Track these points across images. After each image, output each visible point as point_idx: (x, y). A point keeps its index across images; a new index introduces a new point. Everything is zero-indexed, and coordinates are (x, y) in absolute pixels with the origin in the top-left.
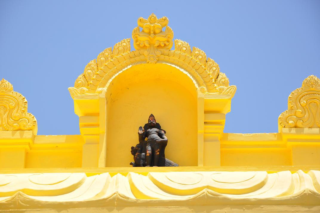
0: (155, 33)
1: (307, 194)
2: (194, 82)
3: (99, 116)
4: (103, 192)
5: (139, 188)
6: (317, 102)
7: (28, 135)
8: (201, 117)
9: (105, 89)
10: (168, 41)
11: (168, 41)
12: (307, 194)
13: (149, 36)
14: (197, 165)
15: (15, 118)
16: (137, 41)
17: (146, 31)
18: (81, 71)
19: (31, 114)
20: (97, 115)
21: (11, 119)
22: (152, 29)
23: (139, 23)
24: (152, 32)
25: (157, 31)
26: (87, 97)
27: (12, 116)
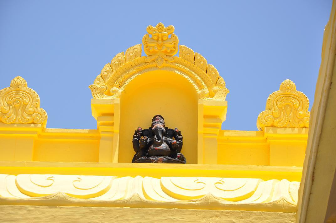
0: (163, 40)
1: (173, 144)
2: (191, 81)
3: (113, 116)
4: (8, 176)
5: (165, 186)
6: (290, 104)
7: (38, 128)
8: (201, 121)
9: (121, 90)
10: (174, 48)
11: (174, 48)
12: (173, 144)
13: (156, 42)
14: (197, 163)
15: (29, 112)
16: (147, 47)
17: (156, 38)
18: (99, 72)
19: (43, 109)
20: (112, 115)
21: (25, 112)
22: (160, 36)
23: (148, 31)
24: (160, 39)
25: (165, 38)
26: (106, 99)
27: (26, 109)
